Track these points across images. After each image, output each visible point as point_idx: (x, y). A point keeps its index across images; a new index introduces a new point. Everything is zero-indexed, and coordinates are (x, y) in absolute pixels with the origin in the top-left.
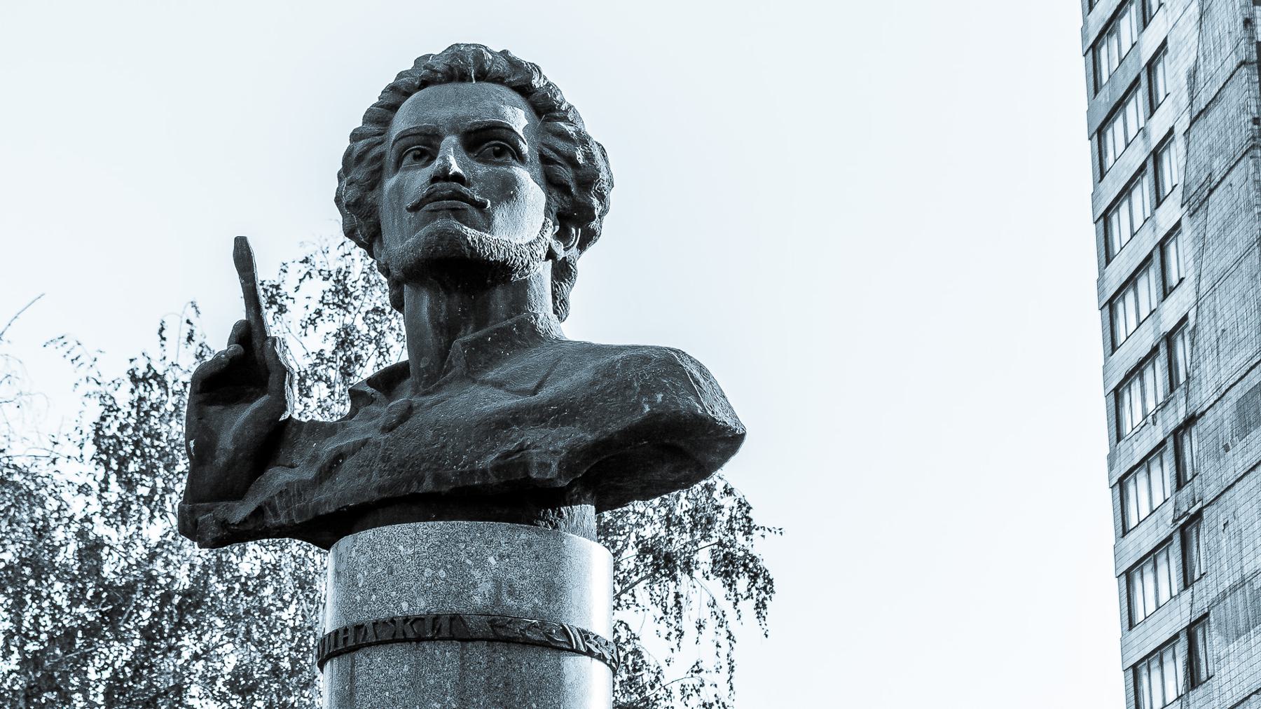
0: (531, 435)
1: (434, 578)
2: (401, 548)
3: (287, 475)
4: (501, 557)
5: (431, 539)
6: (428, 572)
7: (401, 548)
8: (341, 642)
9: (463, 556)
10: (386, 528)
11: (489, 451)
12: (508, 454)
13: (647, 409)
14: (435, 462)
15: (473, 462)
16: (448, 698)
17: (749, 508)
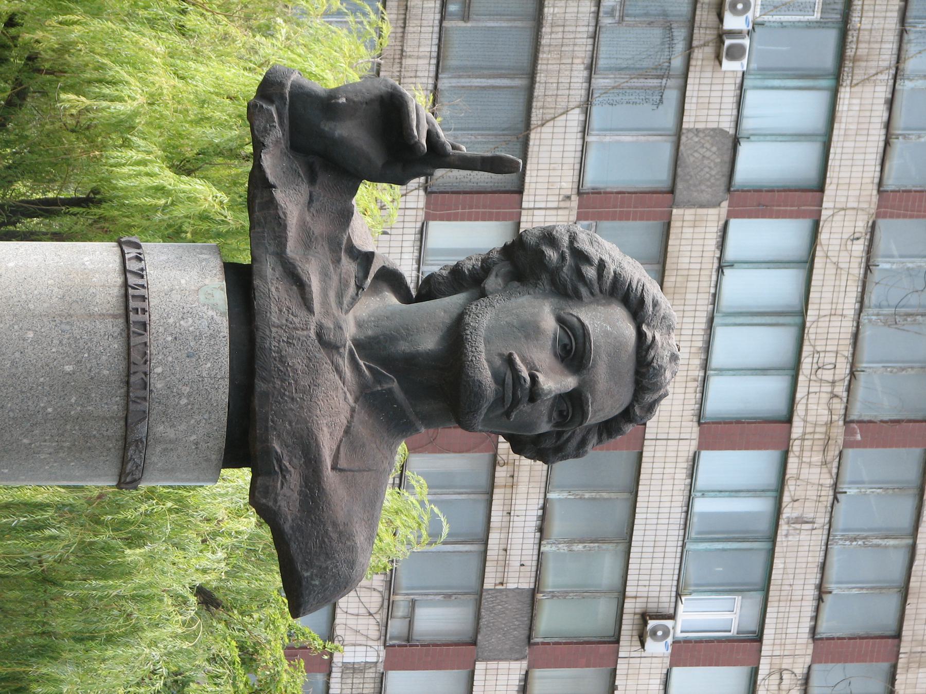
0: (294, 479)
1: (180, 395)
2: (209, 365)
3: (294, 221)
4: (197, 444)
5: (213, 391)
7: (209, 365)
8: (137, 293)
9: (198, 418)
10: (227, 349)
11: (285, 445)
12: (279, 461)
13: (306, 574)
14: (279, 391)
15: (275, 429)
16: (79, 408)
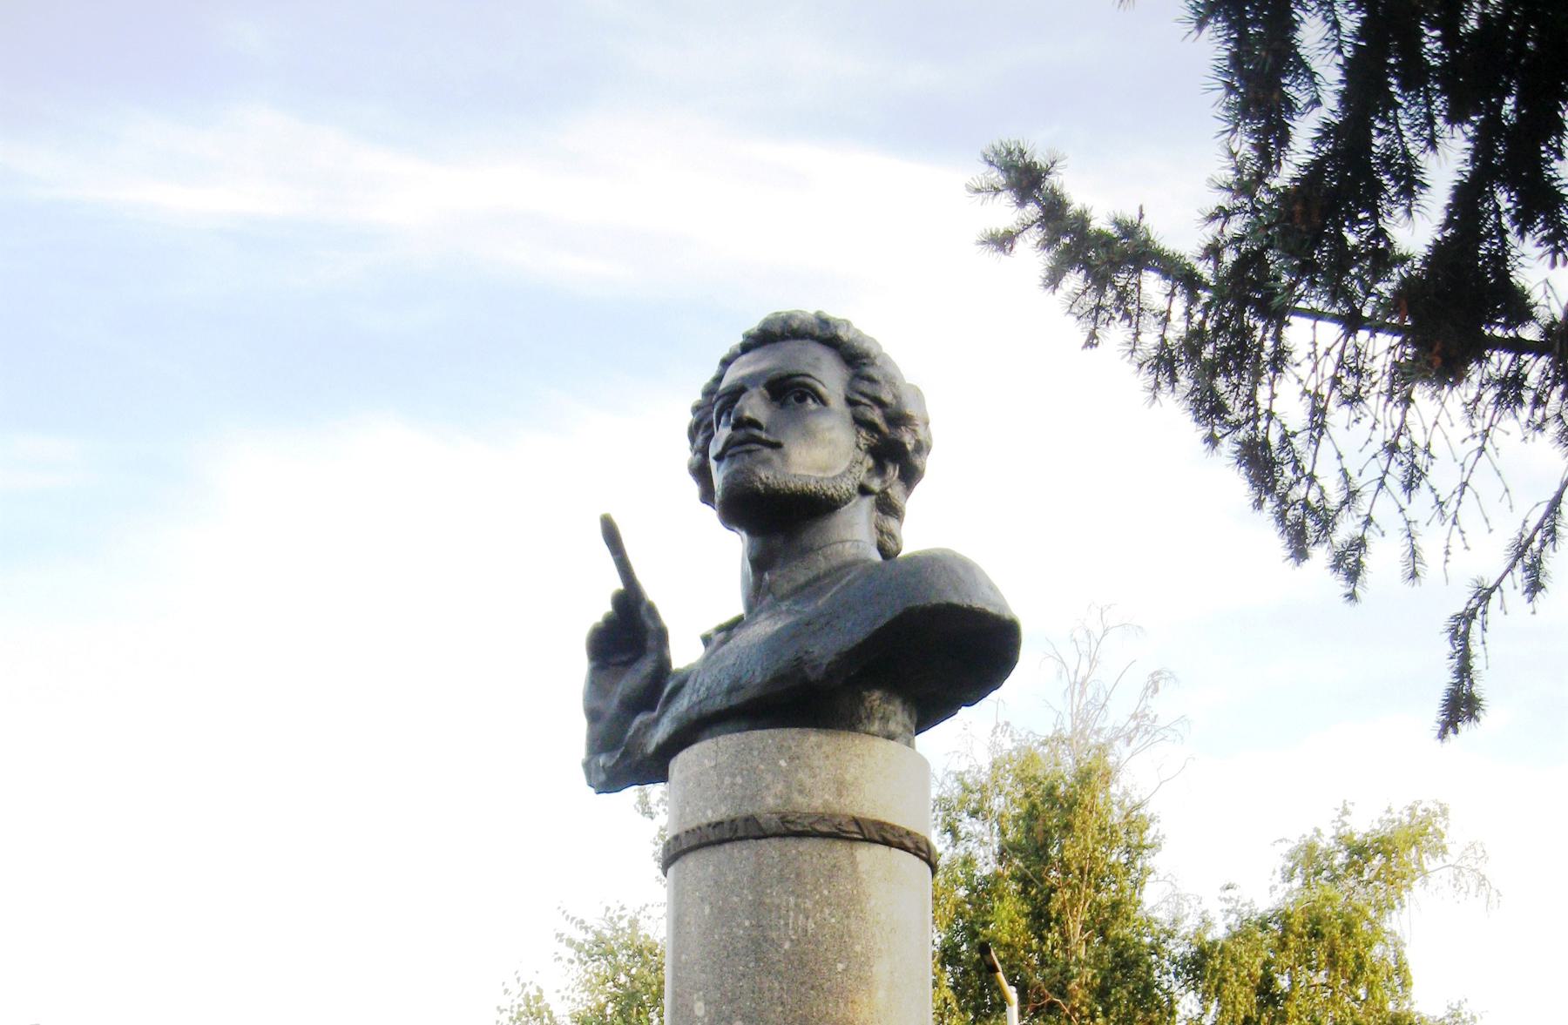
4: (792, 759)
6: (727, 780)
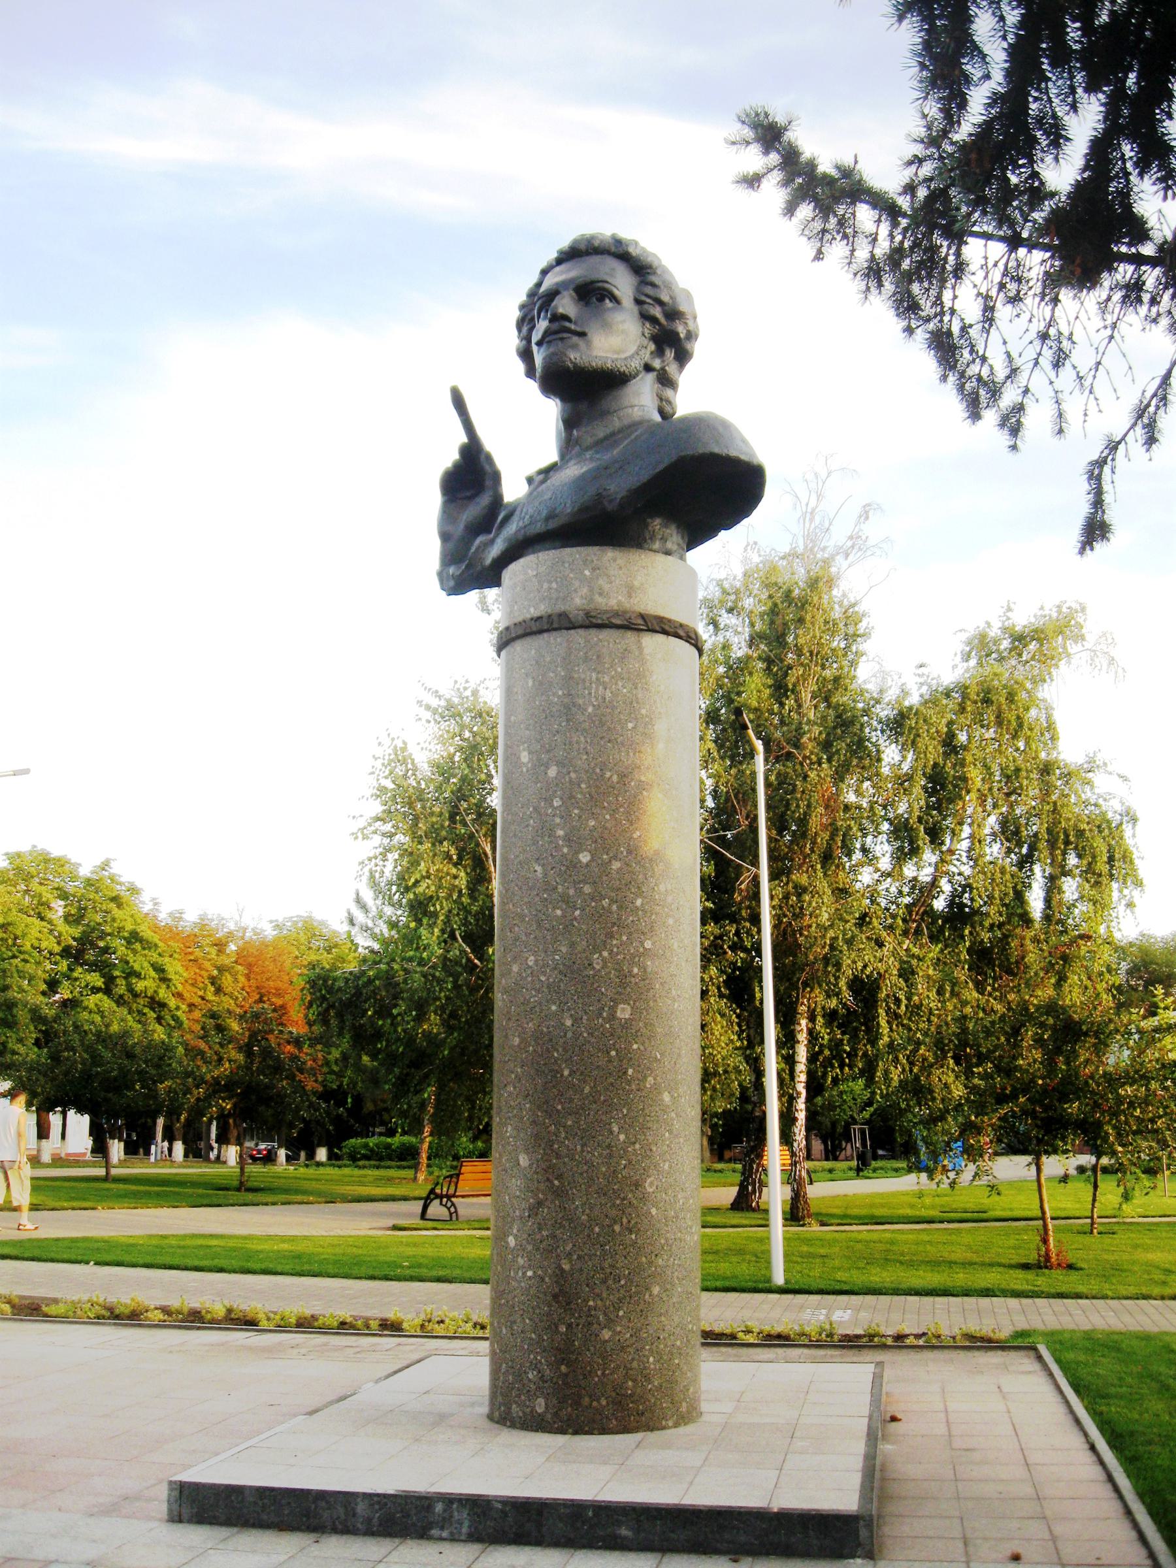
6: (546, 586)
17: (484, 1155)
